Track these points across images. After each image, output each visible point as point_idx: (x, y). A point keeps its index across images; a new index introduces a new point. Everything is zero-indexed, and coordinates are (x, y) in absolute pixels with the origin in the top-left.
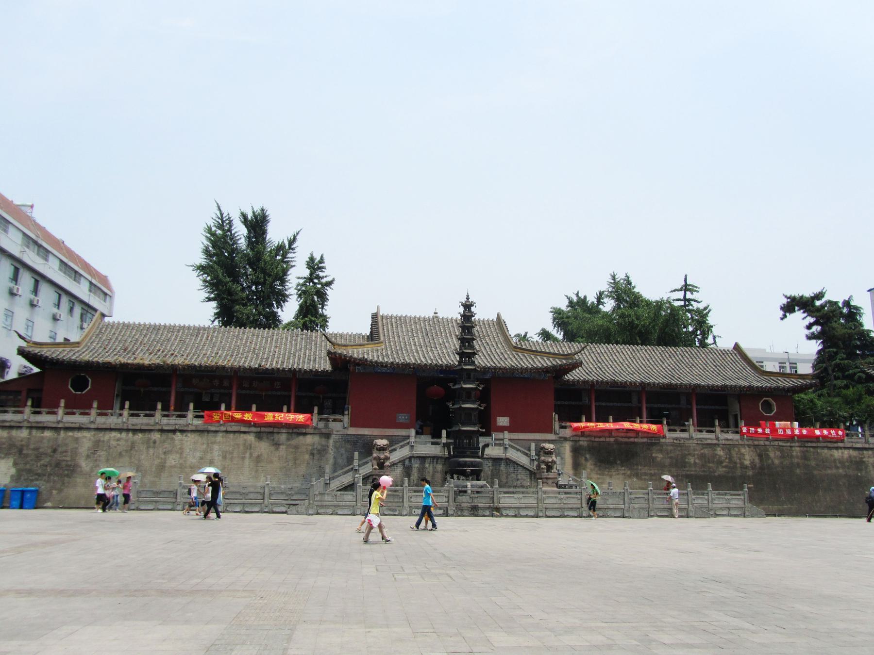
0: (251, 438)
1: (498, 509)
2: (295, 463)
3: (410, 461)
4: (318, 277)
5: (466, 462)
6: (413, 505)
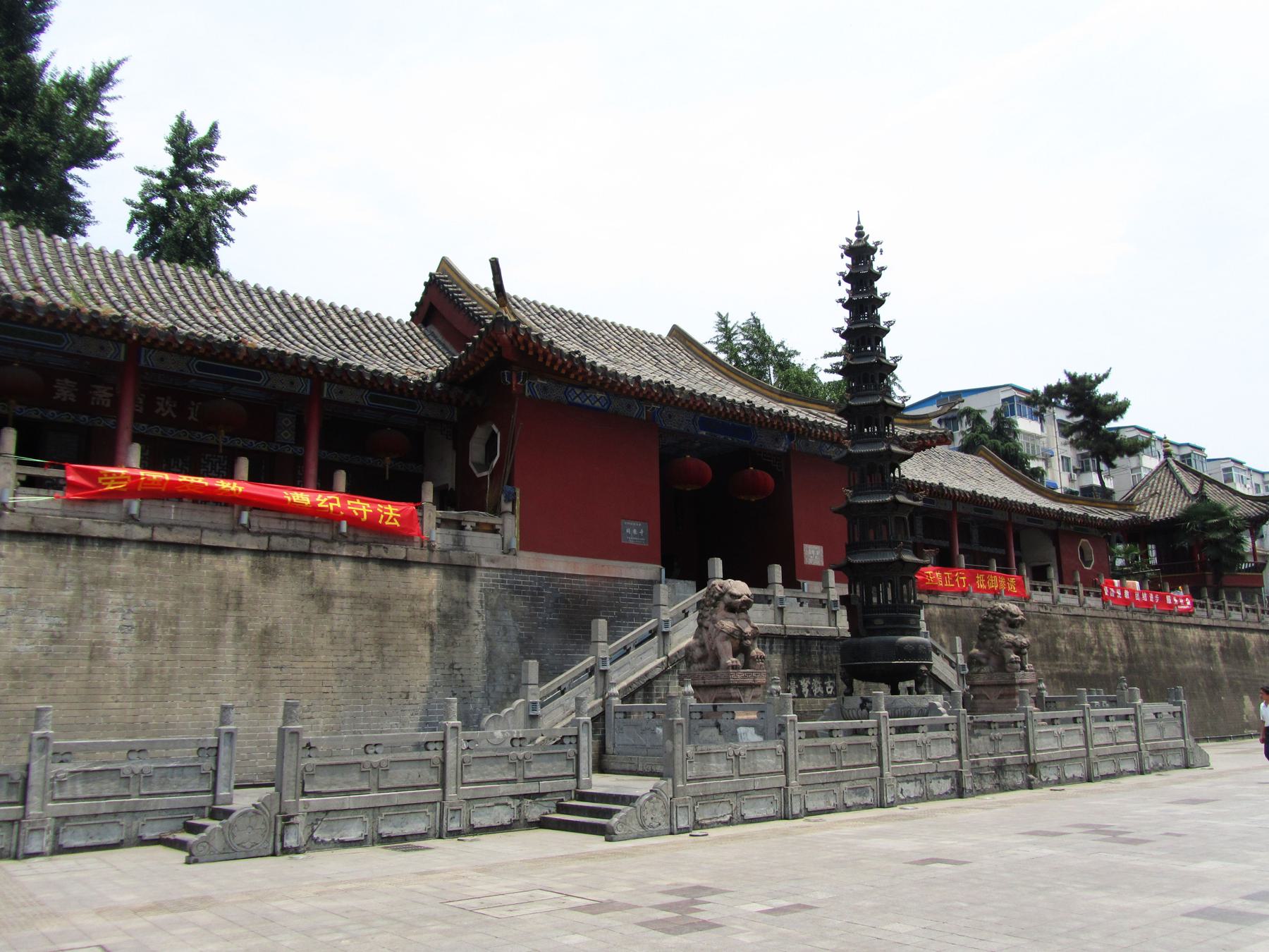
0: (239, 566)
2: (381, 655)
4: (191, 181)
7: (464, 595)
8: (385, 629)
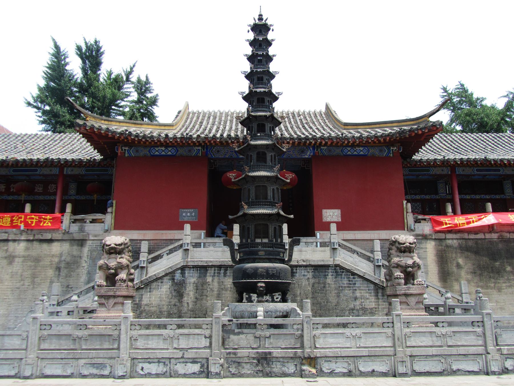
1: (312, 361)
2: (33, 282)
3: (183, 274)
5: (257, 269)
6: (140, 354)
7: (79, 253)
8: (36, 271)
